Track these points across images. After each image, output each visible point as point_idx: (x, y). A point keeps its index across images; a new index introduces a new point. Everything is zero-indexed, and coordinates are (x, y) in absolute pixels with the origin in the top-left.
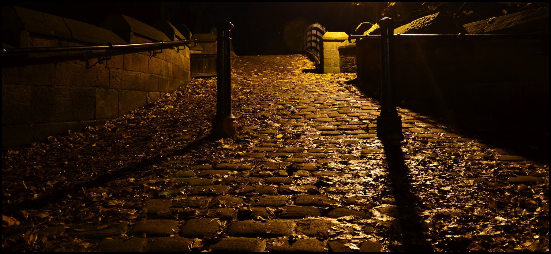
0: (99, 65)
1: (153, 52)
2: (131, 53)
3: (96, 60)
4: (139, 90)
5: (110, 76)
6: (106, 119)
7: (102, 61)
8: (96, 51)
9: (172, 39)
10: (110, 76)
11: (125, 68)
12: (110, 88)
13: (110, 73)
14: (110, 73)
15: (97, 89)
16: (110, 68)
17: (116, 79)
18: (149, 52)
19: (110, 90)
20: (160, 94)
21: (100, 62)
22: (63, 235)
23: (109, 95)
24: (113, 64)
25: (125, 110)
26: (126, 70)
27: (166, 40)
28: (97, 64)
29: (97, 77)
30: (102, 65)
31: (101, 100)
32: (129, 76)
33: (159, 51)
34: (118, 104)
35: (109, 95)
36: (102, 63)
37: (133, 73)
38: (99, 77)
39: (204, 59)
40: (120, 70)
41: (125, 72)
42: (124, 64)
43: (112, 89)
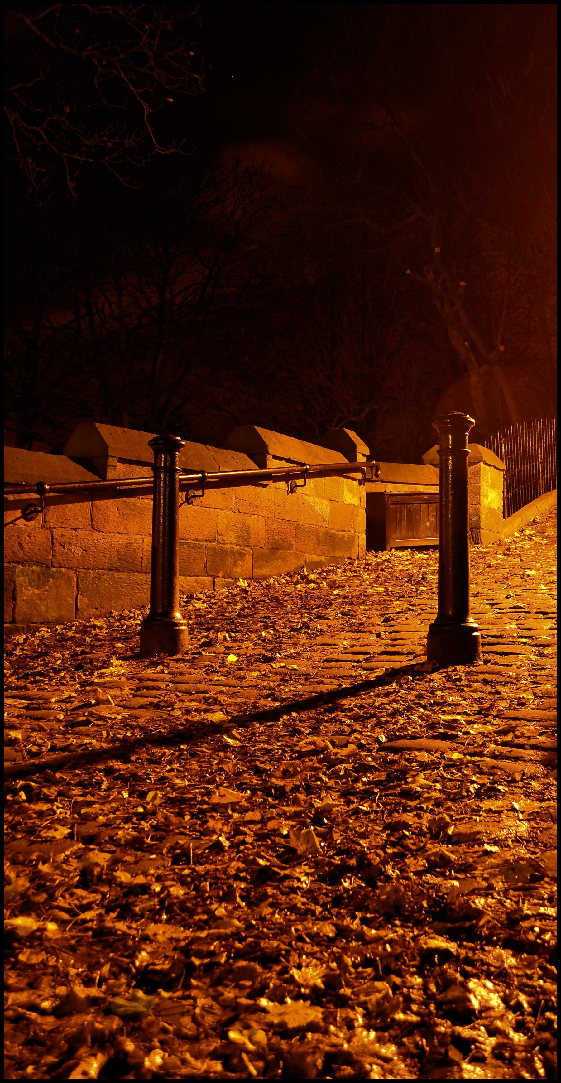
0: (25, 522)
1: (187, 495)
2: (113, 497)
3: (18, 513)
4: (138, 572)
5: (53, 543)
6: (41, 623)
7: (31, 515)
8: (122, 488)
9: (262, 464)
10: (53, 543)
11: (95, 527)
12: (54, 567)
13: (52, 538)
14: (52, 538)
15: (20, 566)
16: (55, 528)
17: (69, 549)
18: (287, 482)
19: (53, 569)
20: (214, 582)
21: (26, 516)
22: (449, 1030)
23: (51, 580)
24: (61, 520)
25: (97, 609)
26: (99, 531)
27: (251, 468)
28: (17, 522)
29: (20, 544)
30: (33, 522)
31: (30, 588)
32: (108, 544)
33: (200, 493)
34: (77, 597)
35: (51, 580)
36: (31, 519)
37: (123, 539)
38: (24, 544)
39: (424, 506)
40: (82, 533)
41: (95, 535)
42: (92, 520)
43: (60, 567)
